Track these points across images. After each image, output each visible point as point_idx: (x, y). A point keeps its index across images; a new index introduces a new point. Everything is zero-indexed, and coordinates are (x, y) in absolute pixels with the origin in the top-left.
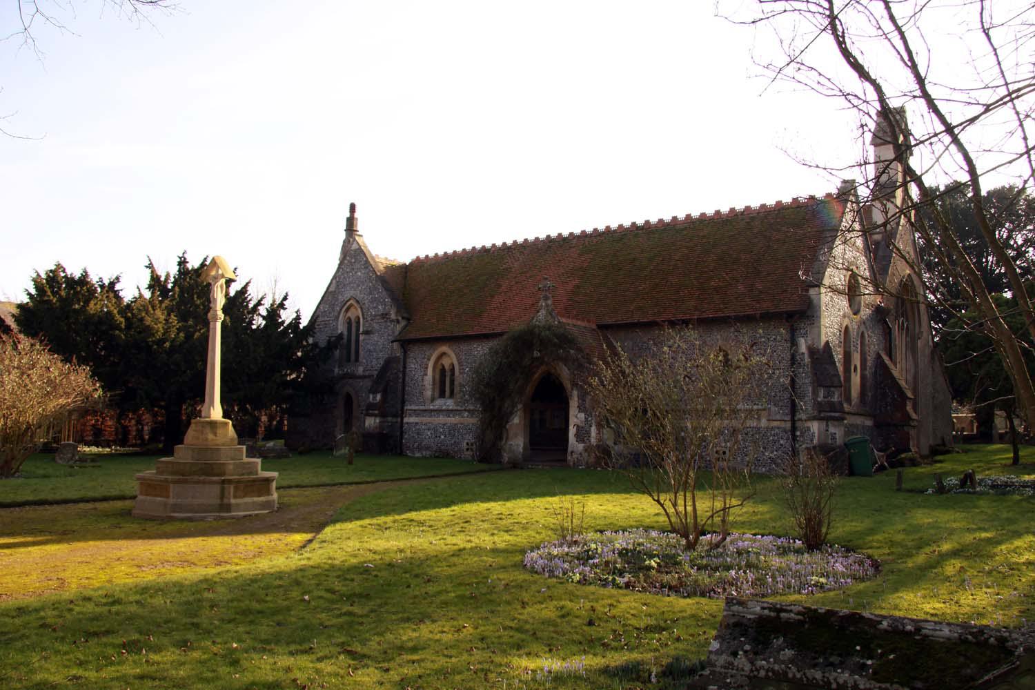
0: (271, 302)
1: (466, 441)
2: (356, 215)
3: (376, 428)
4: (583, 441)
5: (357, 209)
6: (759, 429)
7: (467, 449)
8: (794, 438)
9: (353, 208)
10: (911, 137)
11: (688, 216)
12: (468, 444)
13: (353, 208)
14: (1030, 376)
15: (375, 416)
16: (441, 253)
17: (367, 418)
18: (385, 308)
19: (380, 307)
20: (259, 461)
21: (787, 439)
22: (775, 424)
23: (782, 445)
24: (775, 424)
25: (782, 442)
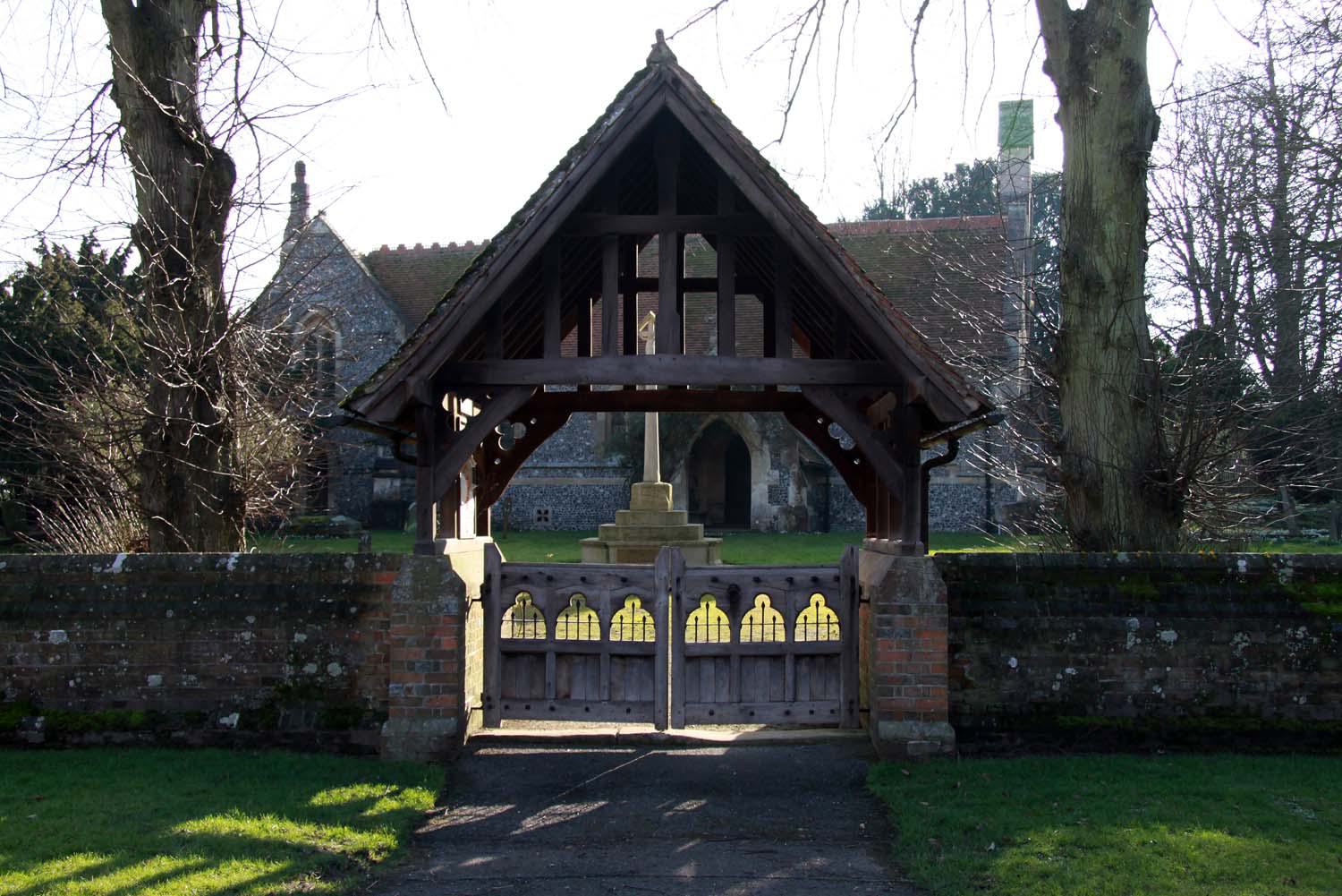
0: (891, 196)
1: (536, 509)
2: (307, 180)
3: (396, 493)
4: (778, 503)
5: (307, 169)
6: (947, 486)
7: (539, 519)
8: (989, 495)
9: (300, 169)
10: (1151, 9)
11: (419, 246)
12: (539, 512)
13: (300, 169)
14: (943, 435)
15: (393, 477)
16: (427, 245)
17: (946, 444)
18: (383, 325)
19: (374, 322)
20: (701, 526)
21: (982, 496)
22: (966, 480)
23: (974, 503)
24: (966, 480)
25: (974, 500)
